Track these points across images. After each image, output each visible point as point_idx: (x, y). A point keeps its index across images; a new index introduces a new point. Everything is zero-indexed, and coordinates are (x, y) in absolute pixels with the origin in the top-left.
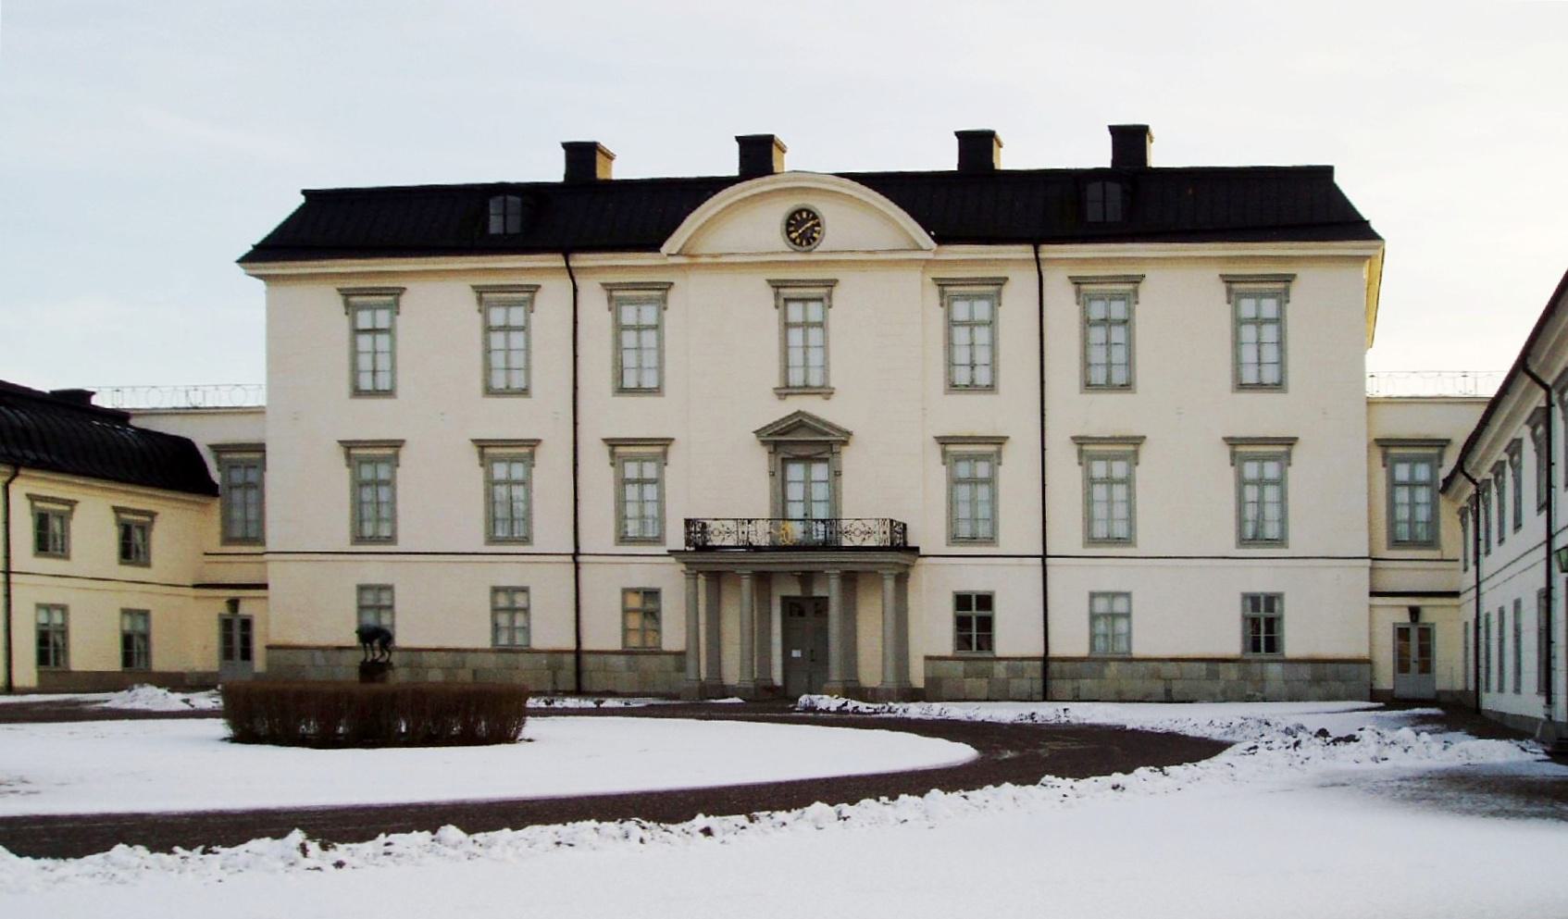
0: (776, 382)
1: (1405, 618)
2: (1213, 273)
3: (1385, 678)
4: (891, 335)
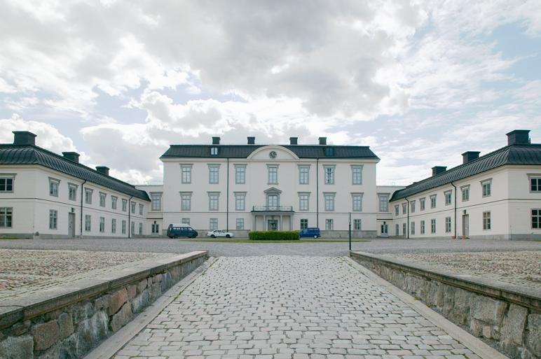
0: (267, 182)
1: (383, 224)
2: (206, 164)
3: (379, 233)
4: (289, 174)
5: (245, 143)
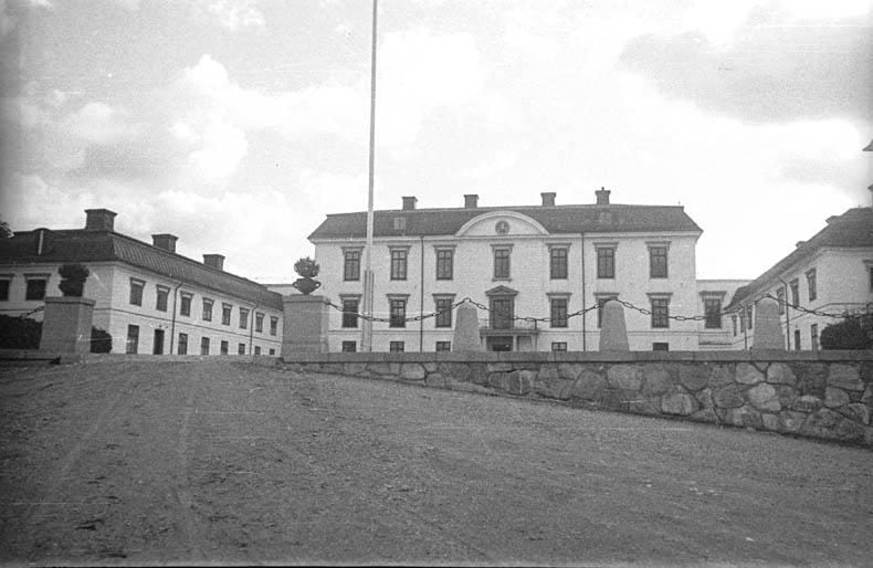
5: (461, 204)
